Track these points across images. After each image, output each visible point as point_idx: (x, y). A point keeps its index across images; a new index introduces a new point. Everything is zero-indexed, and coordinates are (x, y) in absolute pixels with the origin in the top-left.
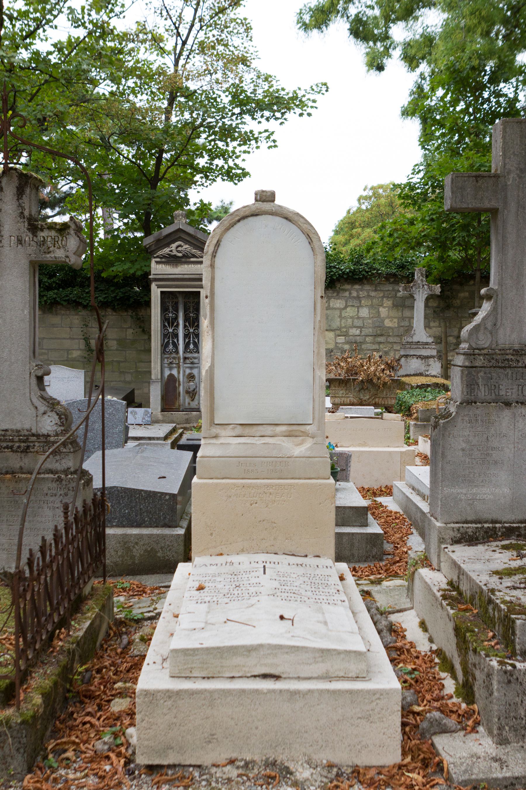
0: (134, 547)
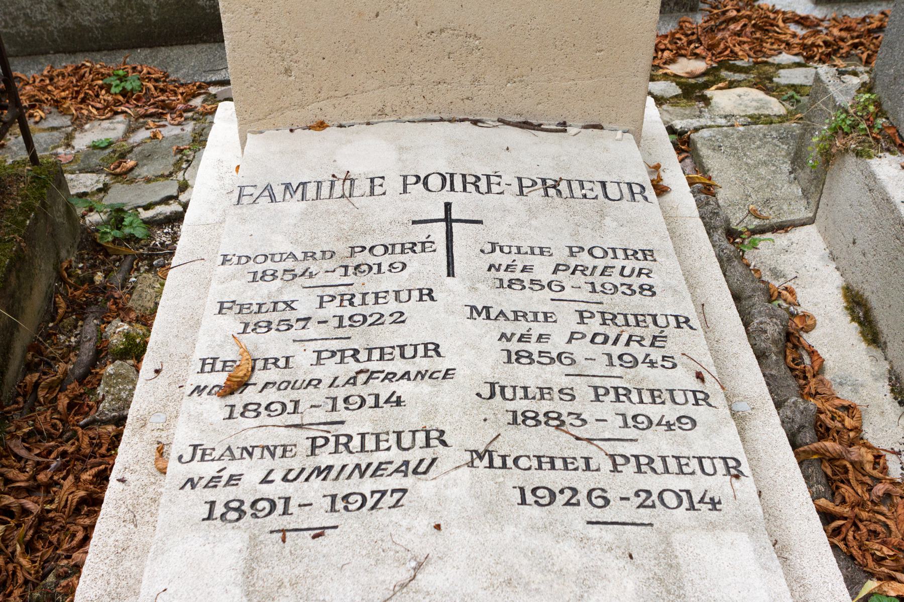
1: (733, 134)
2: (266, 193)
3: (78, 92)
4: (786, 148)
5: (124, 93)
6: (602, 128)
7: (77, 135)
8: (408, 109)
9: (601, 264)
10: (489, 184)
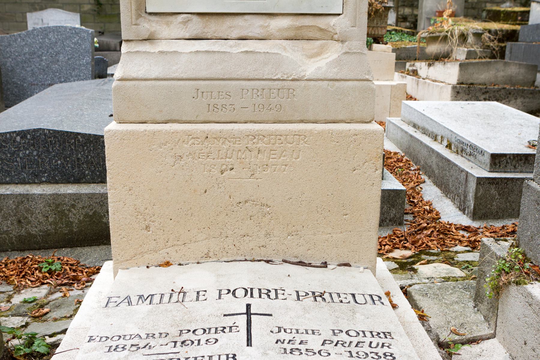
0: (69, 210)
1: (434, 287)
2: (126, 301)
3: (21, 272)
4: (469, 293)
5: (50, 272)
6: (350, 266)
7: (15, 296)
8: (225, 254)
9: (355, 340)
10: (277, 294)
